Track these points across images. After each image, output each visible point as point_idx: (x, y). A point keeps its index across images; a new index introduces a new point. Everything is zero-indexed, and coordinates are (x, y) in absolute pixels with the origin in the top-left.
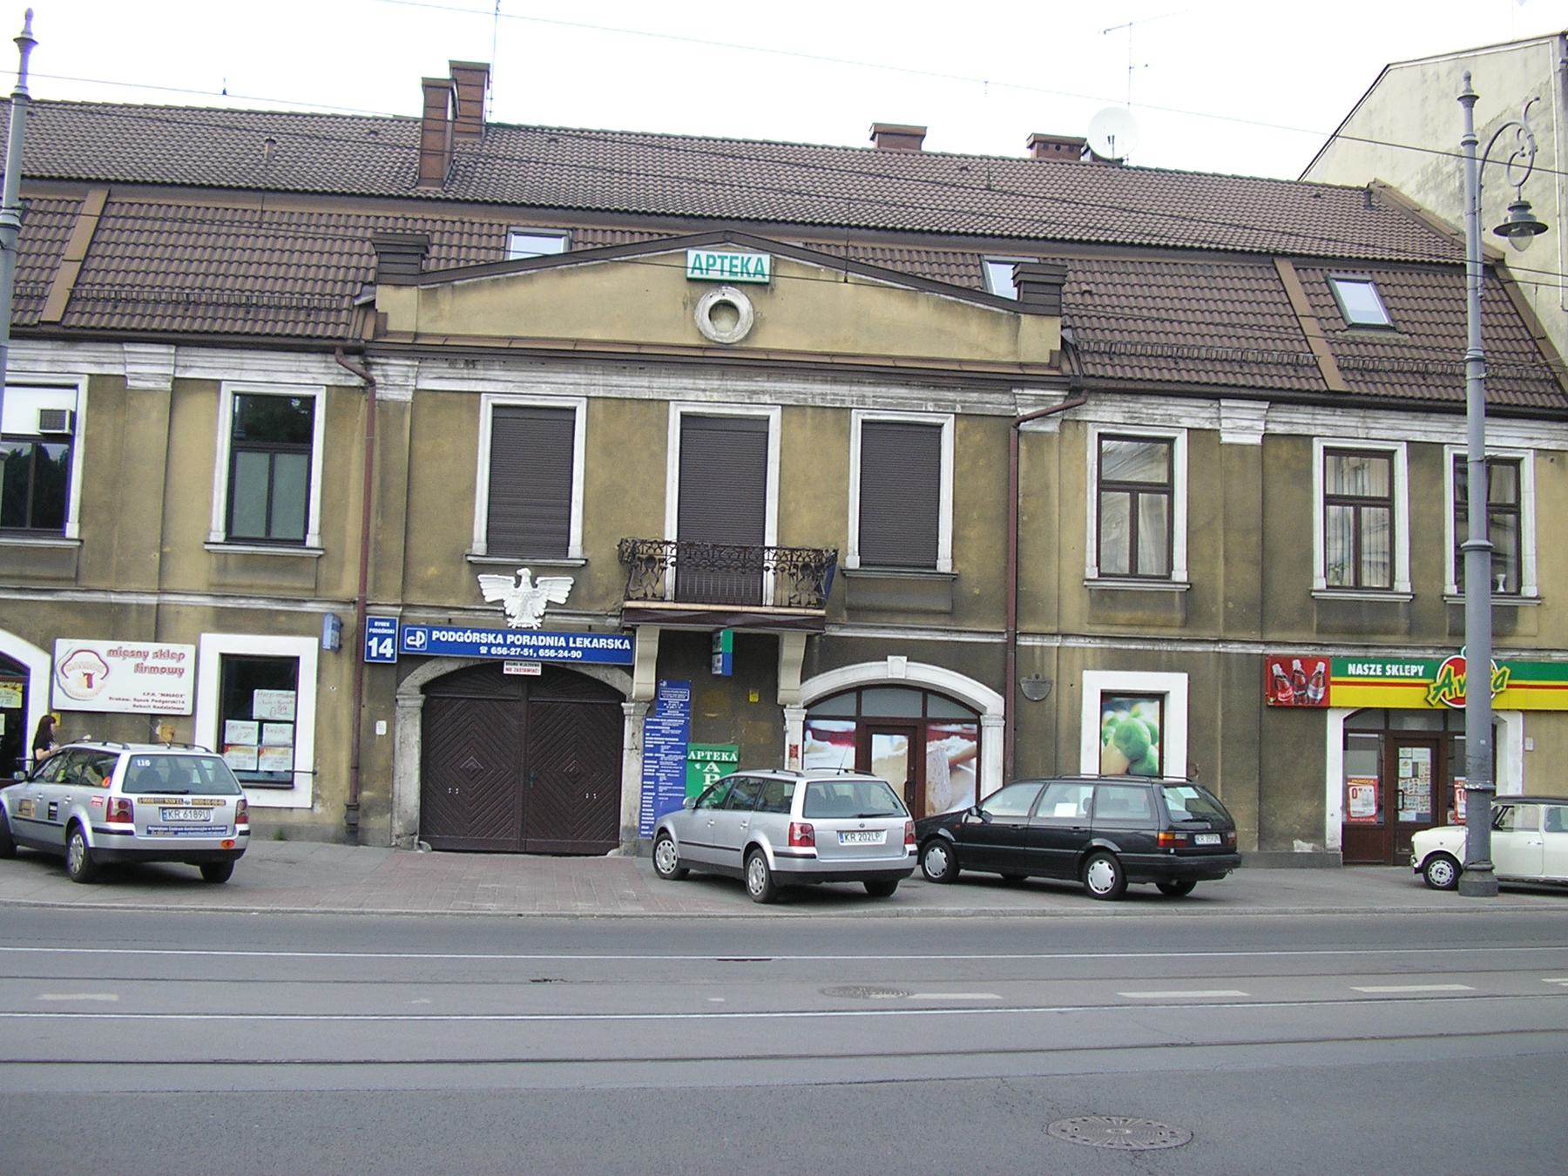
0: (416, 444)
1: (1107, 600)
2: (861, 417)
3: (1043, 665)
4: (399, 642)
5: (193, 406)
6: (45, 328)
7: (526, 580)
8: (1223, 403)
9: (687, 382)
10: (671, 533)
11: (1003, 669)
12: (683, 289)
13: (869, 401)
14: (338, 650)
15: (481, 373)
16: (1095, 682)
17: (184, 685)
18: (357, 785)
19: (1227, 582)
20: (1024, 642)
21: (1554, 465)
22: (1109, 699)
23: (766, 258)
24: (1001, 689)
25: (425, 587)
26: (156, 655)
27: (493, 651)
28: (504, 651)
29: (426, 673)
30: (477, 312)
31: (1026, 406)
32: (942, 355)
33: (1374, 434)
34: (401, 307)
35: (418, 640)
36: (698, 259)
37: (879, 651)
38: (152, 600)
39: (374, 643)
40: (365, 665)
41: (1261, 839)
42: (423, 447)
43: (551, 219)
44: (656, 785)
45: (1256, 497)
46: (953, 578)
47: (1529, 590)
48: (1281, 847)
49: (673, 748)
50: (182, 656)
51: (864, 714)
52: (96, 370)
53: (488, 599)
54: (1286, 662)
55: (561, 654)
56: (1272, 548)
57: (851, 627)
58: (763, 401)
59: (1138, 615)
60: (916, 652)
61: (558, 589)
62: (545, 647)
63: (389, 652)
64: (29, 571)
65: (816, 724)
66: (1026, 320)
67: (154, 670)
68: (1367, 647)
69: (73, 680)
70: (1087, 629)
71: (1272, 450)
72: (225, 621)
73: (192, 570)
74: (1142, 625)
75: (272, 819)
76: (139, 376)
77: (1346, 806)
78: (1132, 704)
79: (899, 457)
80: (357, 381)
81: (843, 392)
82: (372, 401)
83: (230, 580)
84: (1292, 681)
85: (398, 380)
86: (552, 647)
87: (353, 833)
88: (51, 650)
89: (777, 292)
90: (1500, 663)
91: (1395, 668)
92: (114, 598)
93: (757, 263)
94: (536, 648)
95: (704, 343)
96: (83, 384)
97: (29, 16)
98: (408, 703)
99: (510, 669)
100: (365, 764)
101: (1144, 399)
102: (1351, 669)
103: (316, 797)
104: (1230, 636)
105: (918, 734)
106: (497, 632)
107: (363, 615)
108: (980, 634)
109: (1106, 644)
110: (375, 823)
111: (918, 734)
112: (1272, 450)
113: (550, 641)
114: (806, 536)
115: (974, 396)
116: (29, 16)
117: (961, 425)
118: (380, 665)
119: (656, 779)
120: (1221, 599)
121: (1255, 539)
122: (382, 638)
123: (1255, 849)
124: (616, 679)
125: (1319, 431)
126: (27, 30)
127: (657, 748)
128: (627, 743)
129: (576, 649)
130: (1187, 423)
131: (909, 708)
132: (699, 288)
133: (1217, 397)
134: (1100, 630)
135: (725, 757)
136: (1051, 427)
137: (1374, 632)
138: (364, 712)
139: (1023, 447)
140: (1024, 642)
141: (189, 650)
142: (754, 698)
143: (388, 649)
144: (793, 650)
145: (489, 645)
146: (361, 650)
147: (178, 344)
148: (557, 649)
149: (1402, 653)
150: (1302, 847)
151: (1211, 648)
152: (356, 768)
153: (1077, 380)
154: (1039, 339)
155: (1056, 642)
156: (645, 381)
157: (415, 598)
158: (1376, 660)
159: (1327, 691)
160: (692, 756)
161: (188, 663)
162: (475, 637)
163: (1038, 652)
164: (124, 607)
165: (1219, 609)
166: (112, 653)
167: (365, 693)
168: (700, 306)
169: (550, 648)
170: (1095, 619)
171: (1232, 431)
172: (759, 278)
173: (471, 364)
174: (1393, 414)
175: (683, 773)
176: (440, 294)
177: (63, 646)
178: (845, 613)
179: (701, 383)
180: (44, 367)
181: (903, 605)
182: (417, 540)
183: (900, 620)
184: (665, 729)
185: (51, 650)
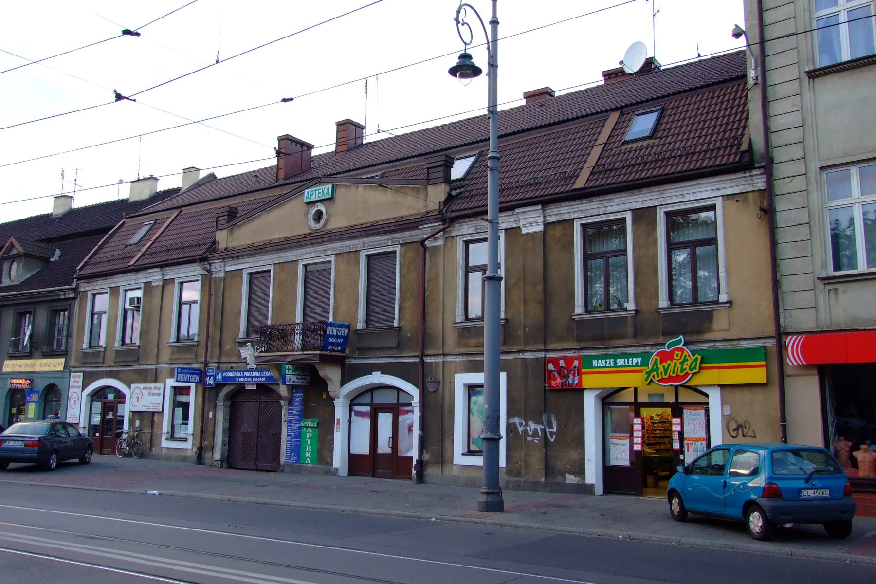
1: (466, 333)
10: (299, 318)
11: (418, 374)
12: (305, 207)
17: (160, 400)
19: (525, 315)
20: (427, 360)
21: (739, 204)
22: (185, 440)
24: (416, 385)
29: (225, 391)
33: (609, 210)
37: (368, 370)
38: (153, 367)
40: (206, 389)
41: (547, 474)
42: (227, 294)
43: (466, 151)
47: (723, 298)
48: (559, 479)
54: (555, 361)
56: (549, 291)
60: (386, 369)
63: (211, 382)
64: (127, 359)
65: (356, 408)
66: (430, 188)
68: (607, 348)
71: (551, 232)
84: (559, 373)
90: (693, 352)
91: (622, 361)
94: (252, 377)
99: (248, 387)
100: (204, 431)
102: (595, 363)
104: (527, 348)
108: (409, 358)
109: (465, 358)
115: (407, 233)
117: (403, 249)
121: (540, 288)
122: (210, 376)
123: (543, 480)
125: (576, 215)
127: (291, 422)
131: (389, 398)
136: (440, 242)
139: (427, 256)
142: (324, 396)
144: (332, 374)
145: (239, 377)
148: (258, 377)
149: (629, 350)
150: (570, 479)
151: (517, 356)
155: (440, 359)
156: (290, 253)
157: (223, 359)
159: (580, 380)
161: (162, 391)
164: (148, 370)
166: (144, 388)
170: (460, 345)
171: (526, 226)
174: (617, 195)
175: (300, 432)
177: (133, 386)
179: (308, 250)
182: (224, 335)
183: (378, 354)
184: (294, 412)
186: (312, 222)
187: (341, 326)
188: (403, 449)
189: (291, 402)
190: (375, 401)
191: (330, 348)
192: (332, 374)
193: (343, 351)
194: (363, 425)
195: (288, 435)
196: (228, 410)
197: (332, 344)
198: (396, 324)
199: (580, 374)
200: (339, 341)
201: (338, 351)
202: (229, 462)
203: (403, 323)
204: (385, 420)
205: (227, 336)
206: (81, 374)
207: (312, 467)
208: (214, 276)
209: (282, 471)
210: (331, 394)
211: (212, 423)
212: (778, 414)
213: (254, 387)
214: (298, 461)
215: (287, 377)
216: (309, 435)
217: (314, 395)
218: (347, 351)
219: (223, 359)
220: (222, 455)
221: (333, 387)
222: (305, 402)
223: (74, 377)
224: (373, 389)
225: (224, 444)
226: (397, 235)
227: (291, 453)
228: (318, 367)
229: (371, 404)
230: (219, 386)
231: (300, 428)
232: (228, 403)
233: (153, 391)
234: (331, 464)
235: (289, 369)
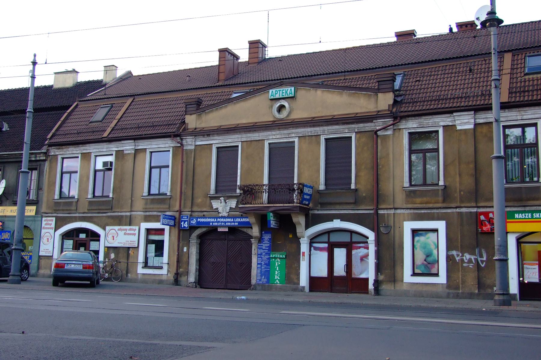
0: (196, 162)
1: (412, 194)
2: (324, 138)
3: (388, 221)
4: (189, 223)
5: (140, 156)
6: (103, 139)
7: (222, 201)
8: (455, 114)
9: (269, 133)
10: (266, 181)
11: (373, 222)
12: (269, 102)
13: (326, 132)
14: (174, 225)
15: (212, 138)
16: (408, 226)
18: (178, 267)
19: (460, 184)
20: (381, 212)
22: (415, 232)
23: (293, 89)
24: (373, 230)
25: (198, 205)
26: (130, 230)
27: (214, 224)
28: (217, 224)
30: (213, 119)
31: (379, 126)
33: (525, 117)
34: (192, 121)
35: (194, 222)
36: (274, 93)
37: (330, 218)
38: (128, 214)
39: (183, 223)
40: (181, 230)
41: (479, 288)
42: (197, 162)
44: (261, 266)
45: (473, 149)
46: (356, 190)
49: (266, 254)
50: (135, 230)
51: (331, 241)
52: (117, 149)
53: (214, 208)
55: (233, 224)
57: (321, 210)
58: (292, 136)
59: (425, 199)
60: (344, 218)
61: (233, 203)
62: (228, 222)
64: (100, 208)
65: (315, 245)
66: (380, 95)
67: (129, 234)
69: (110, 238)
70: (405, 206)
72: (147, 219)
73: (139, 204)
74: (426, 203)
75: (157, 278)
76: (127, 150)
77: (521, 273)
78: (426, 234)
79: (338, 149)
80: (179, 145)
82: (183, 150)
83: (148, 207)
85: (190, 143)
86: (230, 222)
87: (177, 282)
88: (105, 229)
89: (297, 99)
92: (120, 214)
93: (289, 91)
94: (225, 222)
95: (275, 120)
96: (114, 153)
97: (35, 56)
98: (193, 241)
99: (220, 230)
100: (180, 261)
101: (424, 117)
102: (516, 216)
103: (168, 271)
104: (462, 205)
105: (349, 247)
106: (214, 218)
107: (180, 214)
108: (364, 210)
109: (412, 211)
110: (183, 279)
111: (349, 247)
112: (479, 129)
113: (229, 220)
114: (251, 181)
115: (361, 125)
116: (35, 56)
117: (358, 136)
118: (184, 230)
119: (261, 264)
120: (458, 191)
121: (472, 166)
123: (477, 291)
124: (249, 231)
126: (35, 59)
127: (261, 254)
128: (253, 253)
129: (236, 222)
130: (442, 124)
131: (346, 238)
132: (274, 102)
133: (451, 112)
134: (410, 206)
135: (281, 256)
136: (389, 132)
137: (528, 200)
138: (181, 245)
139: (379, 141)
140: (381, 212)
141: (137, 228)
142: (291, 236)
143: (186, 225)
144: (300, 220)
145: (213, 222)
146: (180, 225)
147: (135, 139)
148: (231, 222)
151: (454, 210)
152: (178, 262)
153: (397, 115)
154: (385, 100)
155: (392, 212)
157: (195, 209)
158: (528, 212)
160: (271, 256)
161: (137, 232)
162: (209, 220)
163: (386, 216)
164: (122, 216)
165: (457, 195)
166: (119, 230)
167: (181, 239)
168: (274, 108)
169: (229, 222)
170: (407, 202)
171: (460, 124)
172: (291, 96)
173: (208, 135)
174: (532, 108)
175: (269, 262)
176: (202, 115)
177: (108, 228)
178: (319, 205)
179: (274, 133)
180: (105, 150)
181: (338, 201)
182: (196, 191)
183: (338, 207)
184: (264, 248)
185: (105, 229)
188: (356, 273)
189: (260, 240)
192: (300, 220)
199: (42, 217)
203: (358, 186)
204: (340, 254)
205: (199, 192)
206: (54, 219)
210: (298, 234)
214: (268, 282)
218: (311, 205)
221: (300, 230)
223: (45, 220)
227: (261, 276)
233: (128, 232)
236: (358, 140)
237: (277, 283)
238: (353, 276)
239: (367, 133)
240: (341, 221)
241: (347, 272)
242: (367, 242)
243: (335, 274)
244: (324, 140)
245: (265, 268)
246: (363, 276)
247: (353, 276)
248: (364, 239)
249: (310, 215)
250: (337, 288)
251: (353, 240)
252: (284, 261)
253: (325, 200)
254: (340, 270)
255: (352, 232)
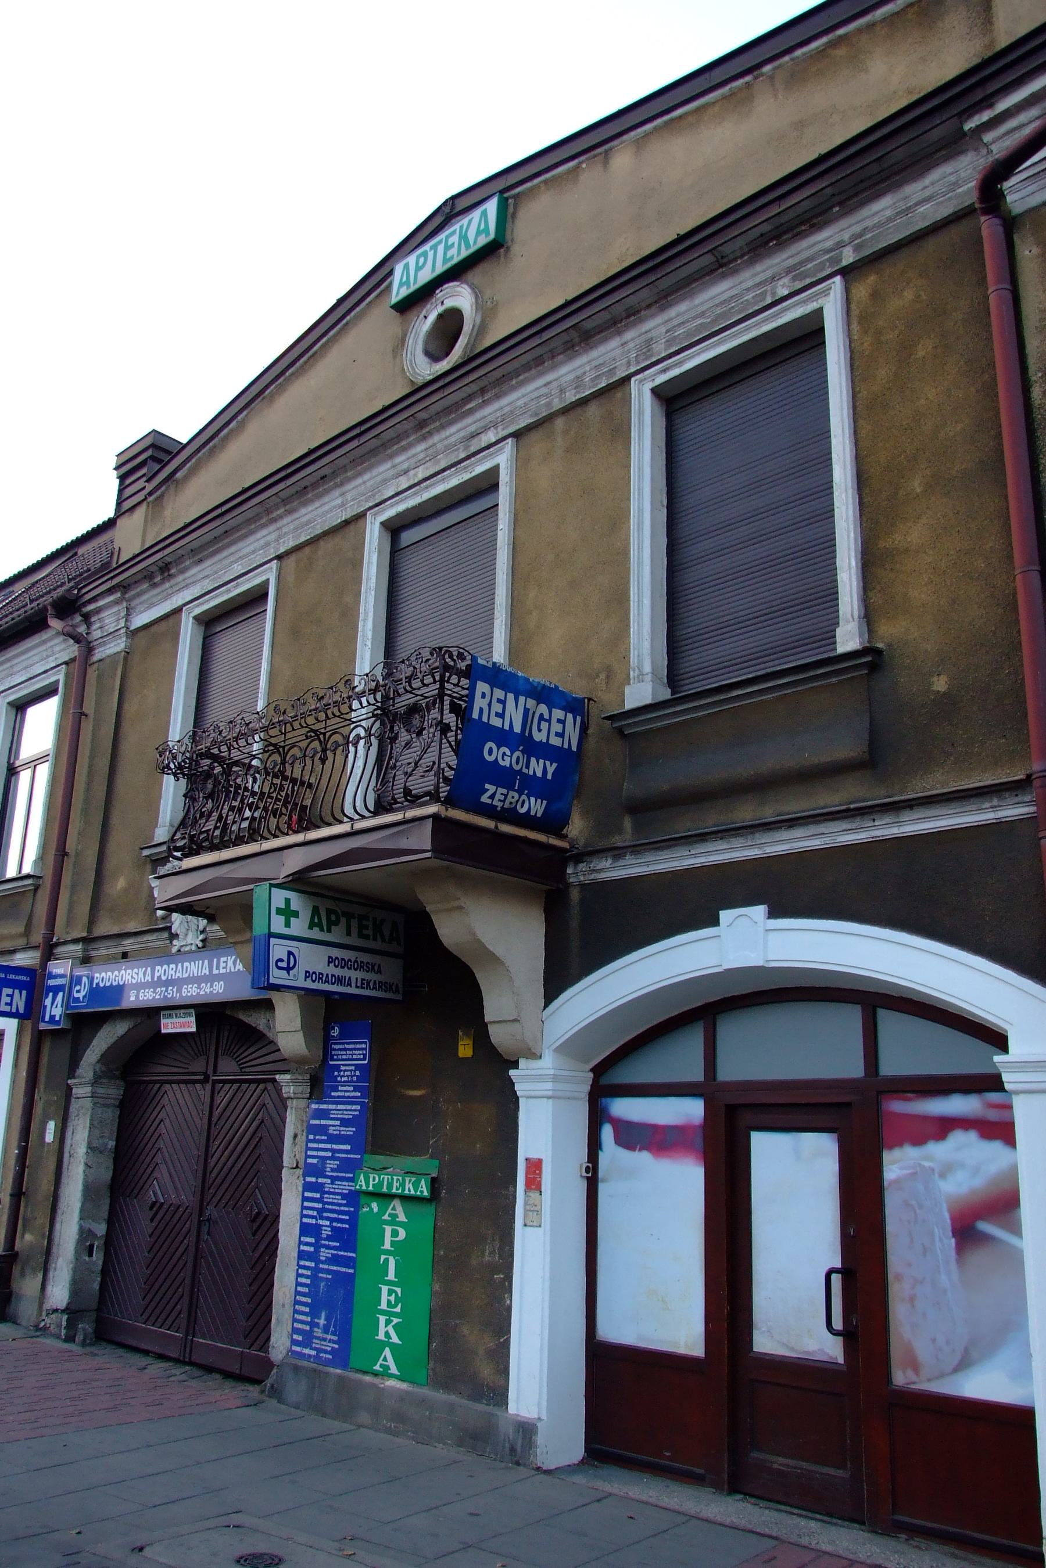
4: (472, 689)
9: (383, 469)
32: (824, 149)
37: (693, 904)
42: (131, 707)
46: (872, 659)
60: (791, 890)
65: (625, 1108)
81: (611, 355)
99: (170, 1025)
105: (861, 1120)
111: (861, 1120)
115: (883, 207)
117: (862, 291)
128: (287, 1160)
131: (821, 1050)
135: (409, 1189)
142: (465, 1050)
144: (500, 934)
160: (361, 1184)
175: (353, 1220)
182: (112, 846)
184: (334, 1126)
186: (421, 360)
187: (544, 694)
188: (923, 1351)
189: (319, 1083)
190: (729, 1071)
191: (492, 794)
192: (500, 934)
193: (554, 822)
194: (663, 1203)
195: (305, 1229)
196: (111, 1115)
197: (505, 777)
198: (848, 638)
200: (536, 767)
201: (527, 821)
202: (99, 1320)
203: (888, 631)
204: (794, 1178)
207: (403, 1397)
208: (98, 654)
209: (276, 1393)
210: (498, 1035)
211: (52, 1166)
212: (603, 1189)
213: (187, 1024)
214: (341, 1357)
215: (279, 950)
216: (393, 1234)
217: (414, 1024)
218: (577, 827)
219: (105, 927)
220: (76, 1289)
221: (509, 999)
222: (378, 1080)
224: (710, 1008)
225: (85, 1244)
226: (825, 238)
227: (314, 1313)
228: (431, 900)
229: (706, 1089)
230: (83, 1023)
231: (354, 1198)
232: (114, 1091)
234: (499, 1395)
235: (287, 913)
236: (863, 319)
237: (385, 1374)
238: (900, 1378)
239: (931, 245)
240: (774, 913)
241: (849, 1335)
242: (993, 1083)
243: (764, 1343)
244: (648, 396)
245: (334, 1260)
246: (985, 1384)
247: (900, 1378)
248: (958, 1056)
249: (575, 895)
250: (779, 1462)
251: (891, 1066)
252: (427, 1216)
253: (667, 775)
254: (794, 1312)
255: (874, 1002)
